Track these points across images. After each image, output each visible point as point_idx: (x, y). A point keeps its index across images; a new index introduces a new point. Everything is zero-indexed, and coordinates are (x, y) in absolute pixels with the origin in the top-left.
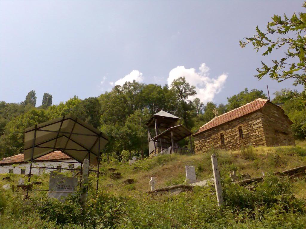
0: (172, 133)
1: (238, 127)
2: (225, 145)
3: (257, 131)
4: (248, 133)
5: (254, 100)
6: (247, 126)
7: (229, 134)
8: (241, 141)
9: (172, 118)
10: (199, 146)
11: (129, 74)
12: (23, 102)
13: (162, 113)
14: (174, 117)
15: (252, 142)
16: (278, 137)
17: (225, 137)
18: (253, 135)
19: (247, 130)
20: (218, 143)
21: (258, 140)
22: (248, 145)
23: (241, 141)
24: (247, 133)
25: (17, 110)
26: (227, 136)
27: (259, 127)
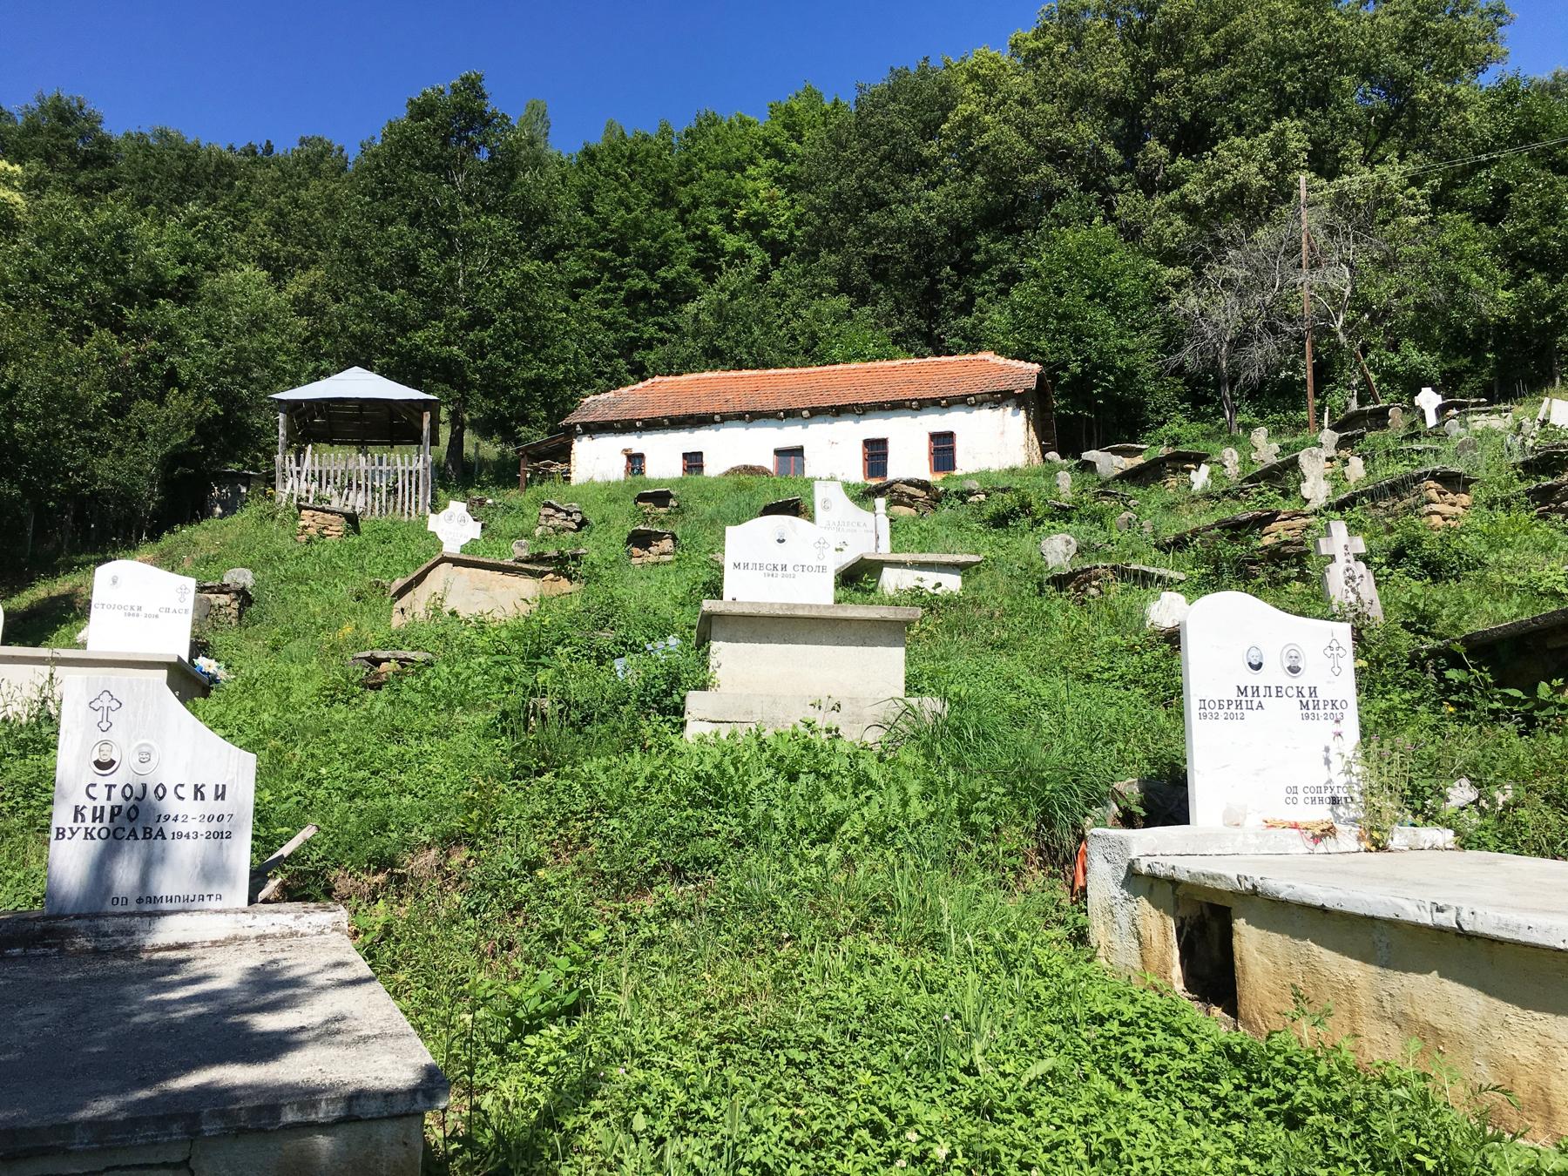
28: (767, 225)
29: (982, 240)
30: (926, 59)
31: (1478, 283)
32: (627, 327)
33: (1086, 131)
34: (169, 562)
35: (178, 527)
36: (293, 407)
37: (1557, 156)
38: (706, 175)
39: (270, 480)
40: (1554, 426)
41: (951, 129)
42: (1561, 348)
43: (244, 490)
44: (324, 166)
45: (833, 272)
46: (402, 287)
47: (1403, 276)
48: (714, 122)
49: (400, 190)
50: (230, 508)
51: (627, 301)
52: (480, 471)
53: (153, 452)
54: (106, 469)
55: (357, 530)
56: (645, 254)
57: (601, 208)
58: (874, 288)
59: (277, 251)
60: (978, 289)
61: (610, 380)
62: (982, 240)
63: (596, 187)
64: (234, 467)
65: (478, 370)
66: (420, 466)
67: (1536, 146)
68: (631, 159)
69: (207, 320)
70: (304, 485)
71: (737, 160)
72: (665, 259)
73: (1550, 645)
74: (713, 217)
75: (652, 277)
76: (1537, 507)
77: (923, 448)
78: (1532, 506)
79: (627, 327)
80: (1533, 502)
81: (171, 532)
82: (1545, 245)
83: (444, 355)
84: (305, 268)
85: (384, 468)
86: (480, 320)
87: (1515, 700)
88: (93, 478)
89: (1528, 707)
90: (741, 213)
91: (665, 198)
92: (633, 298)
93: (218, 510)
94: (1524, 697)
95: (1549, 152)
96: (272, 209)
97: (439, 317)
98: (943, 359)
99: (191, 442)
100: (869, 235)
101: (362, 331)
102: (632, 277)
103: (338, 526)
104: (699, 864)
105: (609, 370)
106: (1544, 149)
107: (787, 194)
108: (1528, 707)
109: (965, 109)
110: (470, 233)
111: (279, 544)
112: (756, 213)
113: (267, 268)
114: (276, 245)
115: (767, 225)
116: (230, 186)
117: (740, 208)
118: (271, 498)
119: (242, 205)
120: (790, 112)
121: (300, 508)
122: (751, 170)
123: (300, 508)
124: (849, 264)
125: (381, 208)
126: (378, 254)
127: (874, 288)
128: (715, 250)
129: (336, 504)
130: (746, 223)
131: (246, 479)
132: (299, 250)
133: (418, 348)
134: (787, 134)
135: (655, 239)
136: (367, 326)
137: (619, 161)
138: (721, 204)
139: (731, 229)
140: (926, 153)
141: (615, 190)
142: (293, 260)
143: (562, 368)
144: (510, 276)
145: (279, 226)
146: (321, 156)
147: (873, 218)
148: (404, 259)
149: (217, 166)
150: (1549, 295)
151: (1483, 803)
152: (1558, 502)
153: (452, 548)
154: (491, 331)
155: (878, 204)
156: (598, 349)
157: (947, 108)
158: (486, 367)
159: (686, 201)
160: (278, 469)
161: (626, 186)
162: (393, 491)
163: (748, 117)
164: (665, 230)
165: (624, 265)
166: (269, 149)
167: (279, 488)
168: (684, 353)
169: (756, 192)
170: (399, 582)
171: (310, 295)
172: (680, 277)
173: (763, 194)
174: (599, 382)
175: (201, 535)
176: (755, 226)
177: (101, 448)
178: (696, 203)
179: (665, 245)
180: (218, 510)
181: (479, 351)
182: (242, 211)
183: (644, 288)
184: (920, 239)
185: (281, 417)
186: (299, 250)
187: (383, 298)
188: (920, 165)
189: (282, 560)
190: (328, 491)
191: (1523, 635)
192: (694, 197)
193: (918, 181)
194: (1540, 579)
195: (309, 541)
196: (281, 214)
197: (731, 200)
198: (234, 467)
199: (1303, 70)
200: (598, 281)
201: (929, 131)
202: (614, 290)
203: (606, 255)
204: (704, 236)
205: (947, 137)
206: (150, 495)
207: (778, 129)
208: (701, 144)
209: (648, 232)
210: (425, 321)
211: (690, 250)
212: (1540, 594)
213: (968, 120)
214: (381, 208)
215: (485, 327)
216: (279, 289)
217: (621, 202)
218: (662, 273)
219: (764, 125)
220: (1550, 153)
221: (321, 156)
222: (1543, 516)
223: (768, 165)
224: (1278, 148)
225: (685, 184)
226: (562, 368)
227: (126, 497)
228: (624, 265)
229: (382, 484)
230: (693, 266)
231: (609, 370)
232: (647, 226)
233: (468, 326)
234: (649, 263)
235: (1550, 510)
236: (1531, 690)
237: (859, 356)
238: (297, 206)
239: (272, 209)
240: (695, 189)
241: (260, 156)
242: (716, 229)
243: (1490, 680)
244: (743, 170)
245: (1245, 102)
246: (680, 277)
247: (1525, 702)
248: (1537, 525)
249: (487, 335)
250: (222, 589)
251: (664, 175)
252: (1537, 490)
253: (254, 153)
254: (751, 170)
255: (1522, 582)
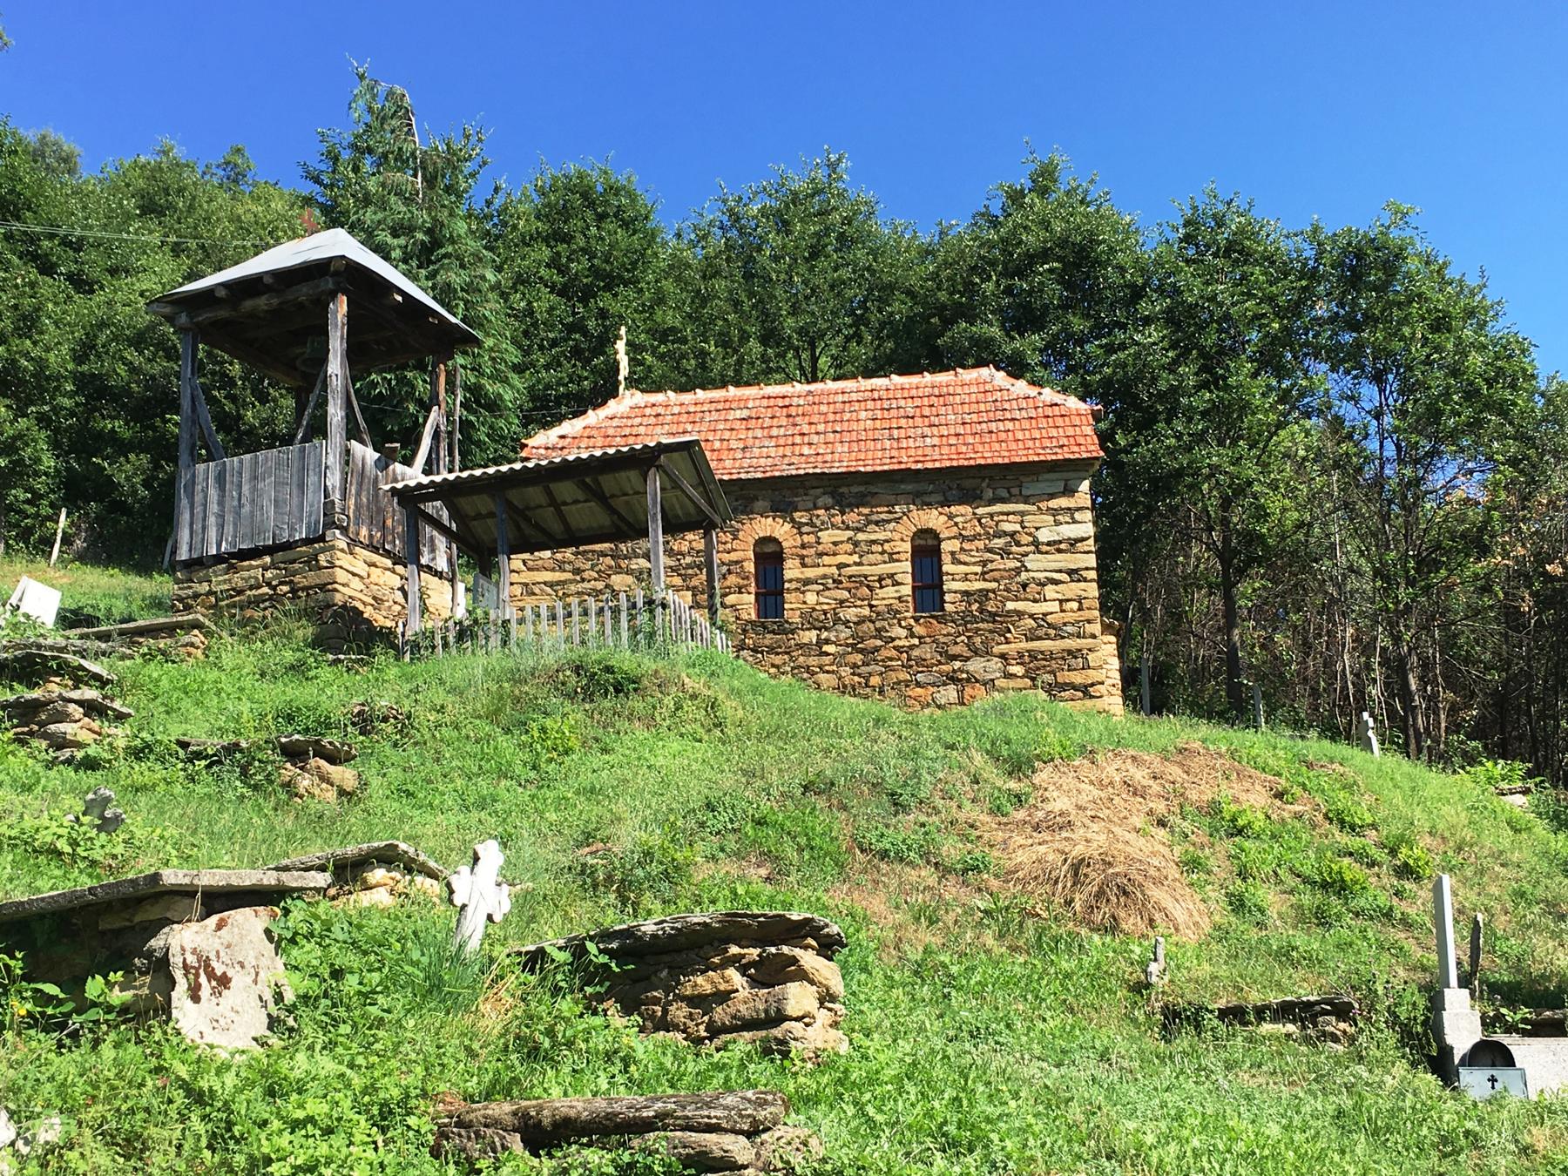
31: (1482, 568)
37: (40, 247)
40: (27, 616)
42: (11, 504)
67: (17, 226)
73: (103, 925)
76: (14, 727)
78: (8, 724)
80: (10, 719)
81: (646, 446)
82: (14, 361)
87: (49, 999)
89: (65, 1009)
94: (62, 996)
95: (33, 239)
104: (278, 1113)
106: (25, 233)
108: (65, 1009)
150: (9, 431)
151: (20, 1144)
152: (42, 724)
191: (73, 909)
194: (37, 830)
212: (35, 851)
220: (32, 242)
222: (20, 741)
235: (31, 734)
236: (75, 985)
243: (19, 972)
247: (60, 1002)
248: (12, 752)
252: (17, 704)
255: (13, 833)
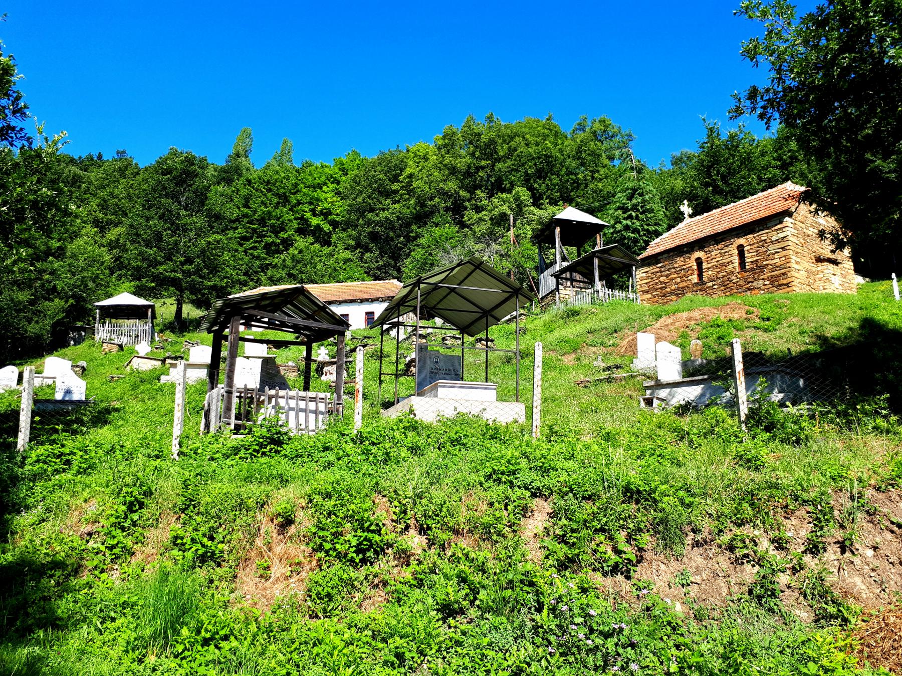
0: (596, 261)
1: (735, 245)
2: (704, 283)
3: (776, 256)
4: (757, 260)
5: (775, 186)
6: (756, 246)
7: (714, 260)
8: (739, 276)
9: (597, 225)
10: (646, 283)
11: (851, 257)
12: (83, 157)
13: (571, 213)
14: (595, 222)
15: (763, 279)
16: (819, 269)
17: (705, 265)
18: (767, 265)
19: (755, 254)
20: (689, 278)
21: (777, 276)
22: (754, 284)
23: (739, 276)
24: (755, 259)
25: (444, 620)
26: (709, 265)
27: (782, 248)
28: (330, 213)
29: (414, 227)
30: (398, 146)
32: (265, 259)
33: (452, 185)
34: (64, 357)
35: (59, 349)
36: (102, 308)
38: (303, 190)
39: (94, 334)
41: (404, 178)
43: (83, 334)
44: (127, 172)
45: (353, 238)
46: (155, 247)
47: (507, 264)
48: (310, 165)
49: (156, 205)
50: (78, 342)
51: (264, 248)
52: (190, 324)
53: (48, 322)
54: (32, 329)
55: (123, 350)
56: (273, 226)
57: (254, 206)
58: (371, 245)
59: (102, 218)
60: (412, 248)
61: (256, 282)
62: (414, 227)
63: (251, 196)
64: (79, 324)
65: (187, 282)
66: (147, 328)
68: (268, 183)
69: (69, 264)
70: (105, 335)
71: (319, 184)
72: (282, 229)
74: (307, 209)
75: (277, 237)
77: (363, 317)
79: (265, 259)
81: (57, 351)
83: (172, 276)
84: (116, 226)
85: (134, 328)
86: (189, 261)
88: (26, 331)
90: (319, 208)
91: (284, 199)
92: (268, 246)
93: (72, 342)
96: (100, 198)
97: (171, 260)
98: (377, 282)
99: (63, 318)
100: (369, 223)
101: (137, 265)
102: (267, 237)
103: (115, 349)
105: (256, 278)
107: (341, 200)
109: (408, 171)
110: (185, 225)
111: (95, 355)
112: (325, 209)
113: (97, 227)
114: (102, 216)
115: (330, 213)
116: (79, 186)
117: (319, 206)
118: (93, 339)
119: (86, 196)
120: (342, 164)
121: (103, 342)
122: (325, 188)
123: (103, 342)
124: (360, 234)
125: (147, 213)
126: (145, 233)
127: (371, 245)
128: (307, 224)
129: (116, 341)
130: (321, 213)
131: (84, 329)
132: (113, 217)
133: (161, 273)
134: (341, 173)
135: (278, 219)
136: (139, 263)
137: (262, 184)
138: (310, 203)
139: (314, 215)
140: (394, 188)
141: (260, 197)
142: (110, 222)
143: (225, 281)
144: (202, 243)
145: (103, 206)
146: (126, 167)
147: (369, 216)
148: (157, 235)
149: (73, 177)
153: (142, 354)
154: (193, 266)
155: (372, 210)
156: (251, 269)
157: (402, 170)
158: (191, 281)
159: (294, 202)
160: (96, 329)
161: (265, 195)
162: (137, 336)
163: (325, 164)
164: (283, 216)
165: (264, 231)
166: (100, 157)
167: (96, 335)
168: (278, 276)
169: (326, 199)
170: (126, 364)
171: (118, 239)
172: (290, 237)
173: (329, 200)
174: (251, 283)
175: (71, 350)
176: (326, 214)
177: (29, 321)
178: (299, 203)
179: (283, 222)
180: (72, 342)
181: (188, 274)
182: (86, 199)
183: (272, 242)
184: (389, 225)
185: (98, 311)
186: (113, 217)
187: (146, 252)
188: (388, 194)
189: (96, 360)
190: (113, 337)
192: (298, 200)
193: (388, 201)
195: (106, 354)
196: (104, 200)
197: (315, 202)
198: (79, 324)
199: (535, 164)
200: (252, 238)
201: (395, 179)
202: (259, 242)
203: (255, 226)
204: (302, 218)
205: (402, 182)
206: (48, 338)
207: (337, 170)
208: (302, 176)
209: (275, 216)
210: (165, 261)
211: (295, 224)
213: (411, 176)
214: (147, 213)
215: (191, 264)
216: (103, 237)
217: (263, 202)
218: (281, 235)
219: (332, 169)
221: (126, 167)
223: (332, 186)
224: (517, 199)
225: (294, 194)
226: (225, 281)
227: (38, 337)
228: (264, 231)
229: (133, 334)
230: (295, 232)
231: (256, 278)
232: (274, 214)
233: (182, 264)
234: (276, 231)
237: (351, 278)
238: (113, 196)
239: (100, 198)
240: (299, 197)
241: (92, 162)
242: (308, 215)
244: (321, 188)
245: (514, 176)
246: (290, 237)
249: (191, 268)
250: (77, 366)
251: (284, 191)
253: (92, 159)
254: (325, 188)
